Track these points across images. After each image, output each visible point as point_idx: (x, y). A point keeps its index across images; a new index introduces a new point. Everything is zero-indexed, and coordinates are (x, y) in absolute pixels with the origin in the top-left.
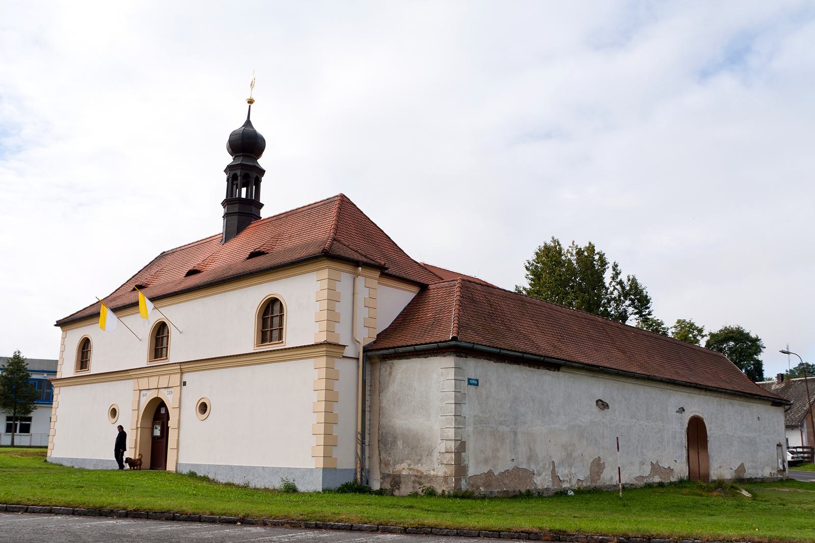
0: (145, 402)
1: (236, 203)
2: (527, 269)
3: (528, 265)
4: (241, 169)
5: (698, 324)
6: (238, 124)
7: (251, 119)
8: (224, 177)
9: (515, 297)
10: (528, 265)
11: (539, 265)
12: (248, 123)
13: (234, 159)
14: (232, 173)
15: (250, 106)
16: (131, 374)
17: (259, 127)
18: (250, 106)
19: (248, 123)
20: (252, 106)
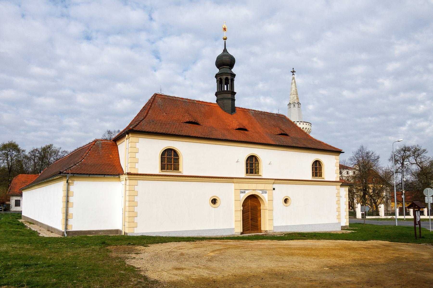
0: (243, 196)
1: (230, 93)
2: (340, 173)
3: (344, 160)
4: (231, 76)
5: (223, 39)
6: (220, 52)
7: (226, 48)
8: (215, 80)
9: (432, 197)
10: (344, 160)
11: (103, 268)
12: (225, 50)
13: (219, 70)
14: (218, 78)
15: (225, 42)
16: (234, 180)
17: (231, 51)
18: (225, 42)
19: (225, 50)
20: (226, 41)
